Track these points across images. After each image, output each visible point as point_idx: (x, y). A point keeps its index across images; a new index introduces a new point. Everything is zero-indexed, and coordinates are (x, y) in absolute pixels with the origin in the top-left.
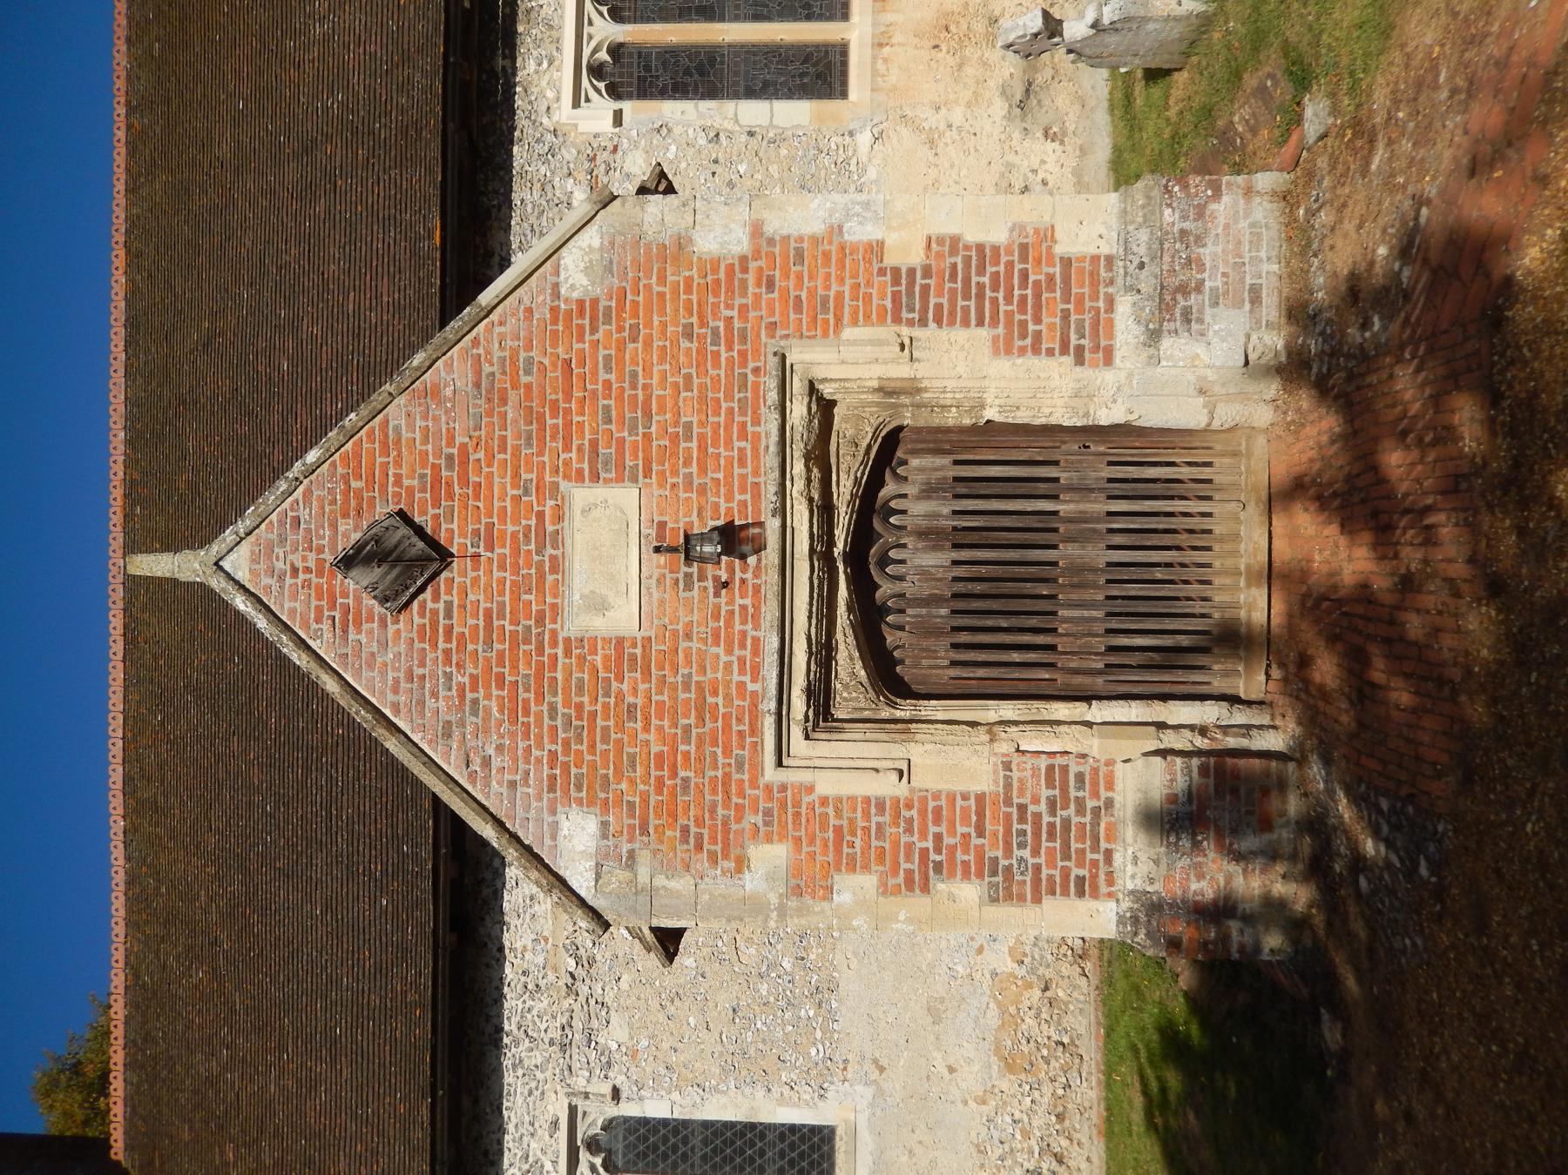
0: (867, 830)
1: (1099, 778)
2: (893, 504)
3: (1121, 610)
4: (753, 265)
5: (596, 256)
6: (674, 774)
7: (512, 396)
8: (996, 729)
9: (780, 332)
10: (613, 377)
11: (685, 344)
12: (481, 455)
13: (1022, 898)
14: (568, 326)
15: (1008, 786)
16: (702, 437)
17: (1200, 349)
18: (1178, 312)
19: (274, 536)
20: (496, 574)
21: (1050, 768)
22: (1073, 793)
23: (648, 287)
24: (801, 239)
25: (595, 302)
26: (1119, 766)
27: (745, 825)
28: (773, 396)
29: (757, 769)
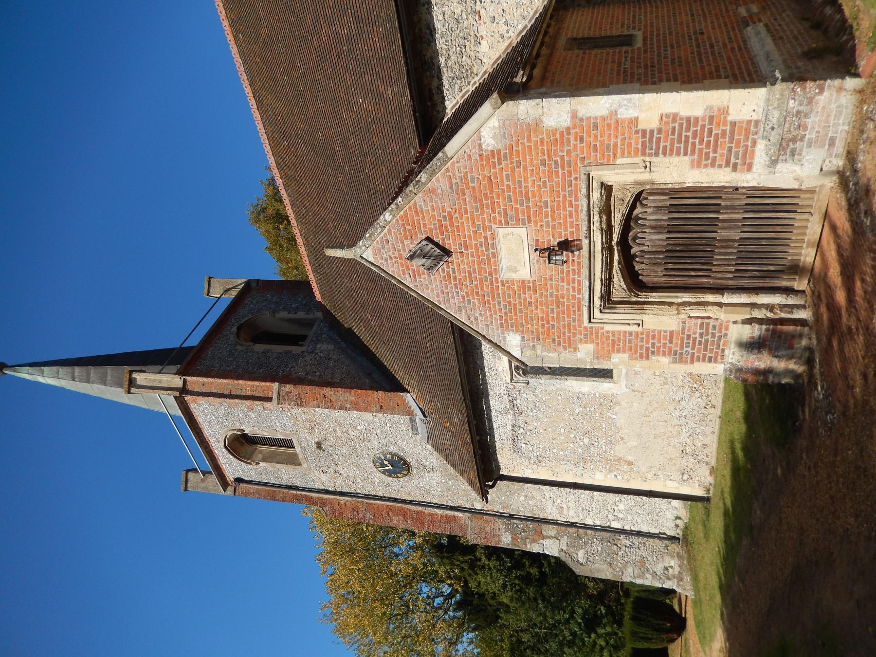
0: (625, 341)
1: (722, 327)
2: (640, 216)
3: (744, 257)
4: (572, 131)
5: (497, 131)
6: (548, 323)
7: (467, 192)
8: (681, 308)
9: (586, 162)
10: (510, 183)
11: (542, 168)
12: (457, 215)
13: (686, 362)
14: (488, 163)
15: (683, 329)
16: (552, 207)
17: (797, 168)
18: (788, 151)
19: (380, 246)
20: (470, 259)
21: (702, 324)
22: (710, 331)
23: (523, 144)
24: (596, 118)
25: (499, 151)
26: (731, 325)
27: (577, 338)
28: (584, 191)
29: (581, 322)
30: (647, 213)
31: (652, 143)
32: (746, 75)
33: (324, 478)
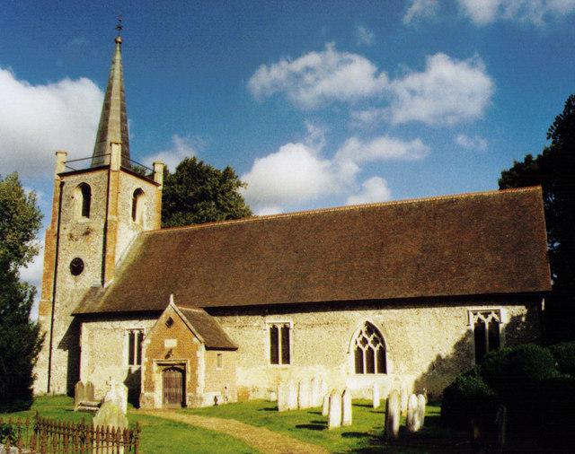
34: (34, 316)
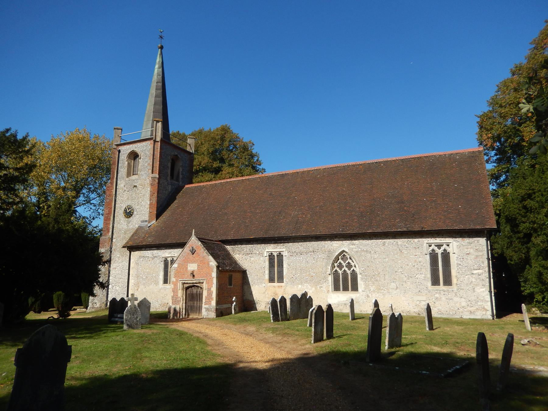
3: (191, 307)
30: (199, 290)
31: (209, 290)
32: (218, 303)
33: (122, 185)
34: (102, 250)
